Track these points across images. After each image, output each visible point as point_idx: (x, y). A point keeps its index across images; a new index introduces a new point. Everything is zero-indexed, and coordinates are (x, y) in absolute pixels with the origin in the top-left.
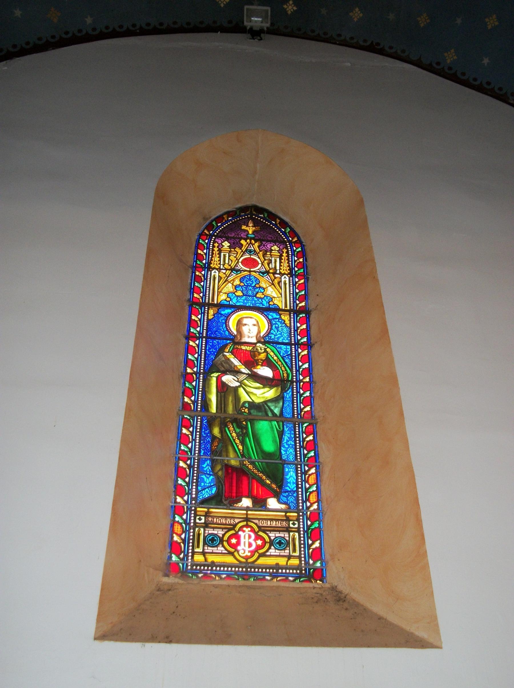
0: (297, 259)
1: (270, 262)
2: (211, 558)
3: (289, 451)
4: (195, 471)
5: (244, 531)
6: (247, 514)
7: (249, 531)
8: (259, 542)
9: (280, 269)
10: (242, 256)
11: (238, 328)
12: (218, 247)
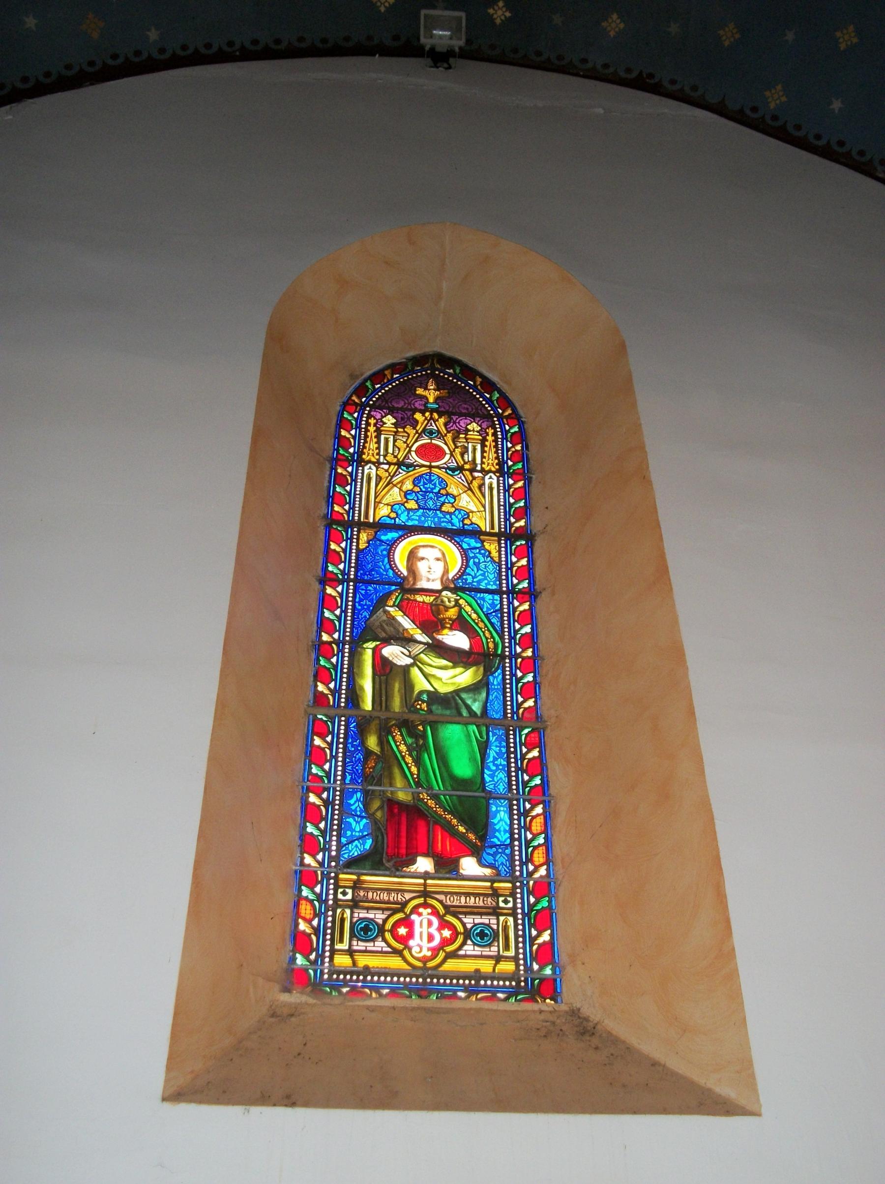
0: (511, 445)
1: (465, 450)
2: (363, 961)
3: (497, 776)
4: (336, 810)
5: (420, 914)
6: (425, 885)
7: (429, 914)
8: (447, 933)
9: (482, 463)
10: (416, 441)
11: (410, 564)
12: (375, 425)
